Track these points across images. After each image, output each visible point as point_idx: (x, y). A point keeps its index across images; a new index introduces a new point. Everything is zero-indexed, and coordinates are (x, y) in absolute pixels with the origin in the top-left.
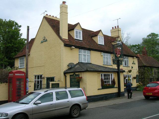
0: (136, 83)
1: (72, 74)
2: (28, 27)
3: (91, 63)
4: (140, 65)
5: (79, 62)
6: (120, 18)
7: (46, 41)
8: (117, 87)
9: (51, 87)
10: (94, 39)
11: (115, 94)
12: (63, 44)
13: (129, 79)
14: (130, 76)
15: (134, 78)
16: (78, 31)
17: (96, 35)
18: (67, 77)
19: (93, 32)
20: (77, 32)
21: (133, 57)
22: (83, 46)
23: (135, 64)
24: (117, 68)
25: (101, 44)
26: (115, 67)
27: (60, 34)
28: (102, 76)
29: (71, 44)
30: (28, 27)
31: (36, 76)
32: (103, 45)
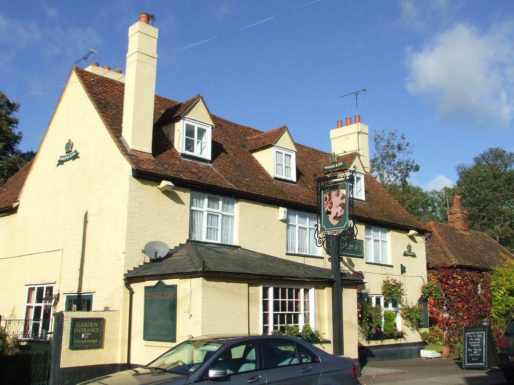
1: (153, 283)
2: (392, 266)
3: (239, 247)
4: (437, 262)
6: (364, 90)
7: (76, 156)
9: (33, 319)
12: (127, 168)
17: (268, 143)
20: (190, 132)
21: (404, 229)
22: (209, 181)
23: (414, 256)
24: (328, 265)
25: (283, 177)
28: (265, 295)
29: (160, 170)
30: (392, 266)
31: (31, 290)
32: (291, 182)
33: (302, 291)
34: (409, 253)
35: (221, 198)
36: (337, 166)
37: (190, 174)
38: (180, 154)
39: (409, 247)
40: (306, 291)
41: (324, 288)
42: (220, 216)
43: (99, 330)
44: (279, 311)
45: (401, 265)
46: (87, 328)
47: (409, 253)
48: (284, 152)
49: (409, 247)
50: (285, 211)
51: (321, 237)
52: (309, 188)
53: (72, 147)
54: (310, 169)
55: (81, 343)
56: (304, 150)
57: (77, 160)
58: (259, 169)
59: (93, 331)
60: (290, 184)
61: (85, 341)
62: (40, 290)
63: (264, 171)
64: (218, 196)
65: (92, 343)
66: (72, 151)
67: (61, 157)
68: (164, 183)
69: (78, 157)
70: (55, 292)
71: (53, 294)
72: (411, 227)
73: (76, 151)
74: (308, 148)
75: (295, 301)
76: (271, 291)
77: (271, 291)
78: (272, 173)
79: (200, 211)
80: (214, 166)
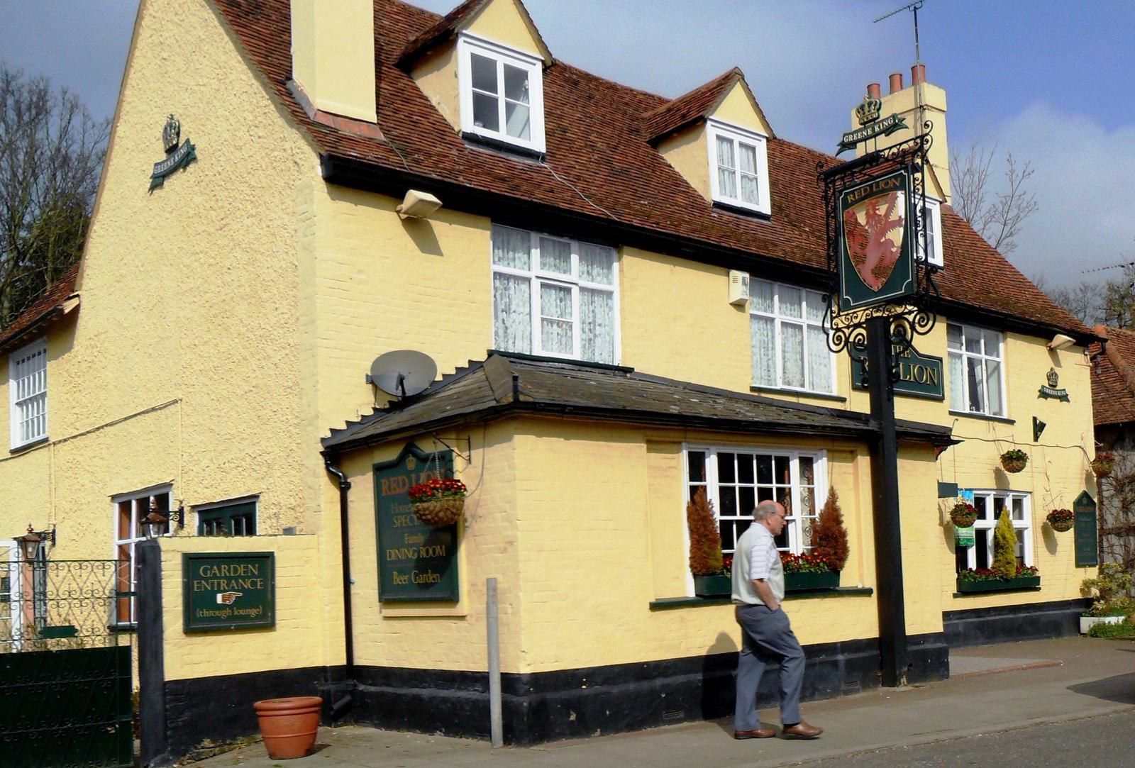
0: (1078, 566)
1: (390, 455)
3: (630, 370)
5: (491, 354)
7: (189, 158)
8: (870, 581)
10: (678, 158)
11: (840, 657)
13: (1010, 526)
14: (1017, 504)
15: (1057, 520)
16: (501, 61)
17: (694, 115)
18: (351, 495)
19: (661, 101)
20: (483, 73)
23: (1064, 398)
26: (861, 403)
27: (300, 76)
28: (697, 470)
29: (404, 164)
31: (125, 508)
33: (795, 465)
34: (1053, 391)
35: (574, 245)
36: (877, 129)
37: (489, 179)
38: (460, 135)
39: (1052, 377)
40: (807, 464)
41: (852, 455)
42: (575, 290)
43: (264, 584)
44: (735, 514)
45: (1035, 419)
46: (229, 579)
47: (1053, 391)
48: (737, 139)
49: (1052, 377)
50: (744, 279)
51: (841, 325)
52: (805, 231)
53: (178, 134)
54: (805, 194)
55: (218, 619)
56: (788, 151)
57: (192, 168)
58: (676, 183)
59: (247, 585)
60: (755, 220)
61: (228, 611)
62: (143, 503)
63: (689, 187)
64: (565, 240)
65: (247, 617)
66: (180, 145)
67: (156, 165)
68: (414, 196)
69: (195, 159)
70: (173, 506)
71: (170, 510)
72: (1059, 327)
73: (188, 141)
74: (798, 148)
75: (778, 489)
76: (711, 465)
77: (711, 465)
78: (715, 194)
79: (517, 279)
80: (555, 169)
